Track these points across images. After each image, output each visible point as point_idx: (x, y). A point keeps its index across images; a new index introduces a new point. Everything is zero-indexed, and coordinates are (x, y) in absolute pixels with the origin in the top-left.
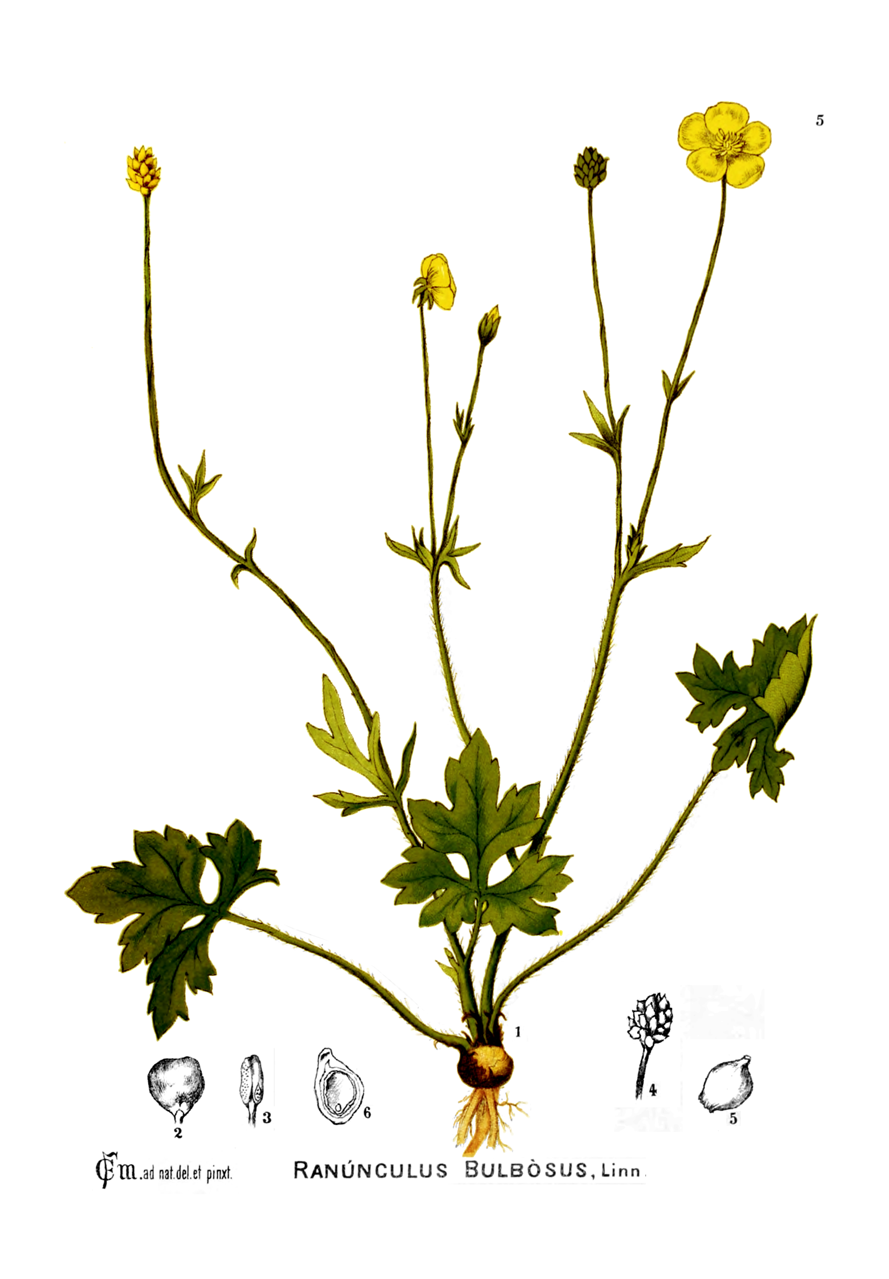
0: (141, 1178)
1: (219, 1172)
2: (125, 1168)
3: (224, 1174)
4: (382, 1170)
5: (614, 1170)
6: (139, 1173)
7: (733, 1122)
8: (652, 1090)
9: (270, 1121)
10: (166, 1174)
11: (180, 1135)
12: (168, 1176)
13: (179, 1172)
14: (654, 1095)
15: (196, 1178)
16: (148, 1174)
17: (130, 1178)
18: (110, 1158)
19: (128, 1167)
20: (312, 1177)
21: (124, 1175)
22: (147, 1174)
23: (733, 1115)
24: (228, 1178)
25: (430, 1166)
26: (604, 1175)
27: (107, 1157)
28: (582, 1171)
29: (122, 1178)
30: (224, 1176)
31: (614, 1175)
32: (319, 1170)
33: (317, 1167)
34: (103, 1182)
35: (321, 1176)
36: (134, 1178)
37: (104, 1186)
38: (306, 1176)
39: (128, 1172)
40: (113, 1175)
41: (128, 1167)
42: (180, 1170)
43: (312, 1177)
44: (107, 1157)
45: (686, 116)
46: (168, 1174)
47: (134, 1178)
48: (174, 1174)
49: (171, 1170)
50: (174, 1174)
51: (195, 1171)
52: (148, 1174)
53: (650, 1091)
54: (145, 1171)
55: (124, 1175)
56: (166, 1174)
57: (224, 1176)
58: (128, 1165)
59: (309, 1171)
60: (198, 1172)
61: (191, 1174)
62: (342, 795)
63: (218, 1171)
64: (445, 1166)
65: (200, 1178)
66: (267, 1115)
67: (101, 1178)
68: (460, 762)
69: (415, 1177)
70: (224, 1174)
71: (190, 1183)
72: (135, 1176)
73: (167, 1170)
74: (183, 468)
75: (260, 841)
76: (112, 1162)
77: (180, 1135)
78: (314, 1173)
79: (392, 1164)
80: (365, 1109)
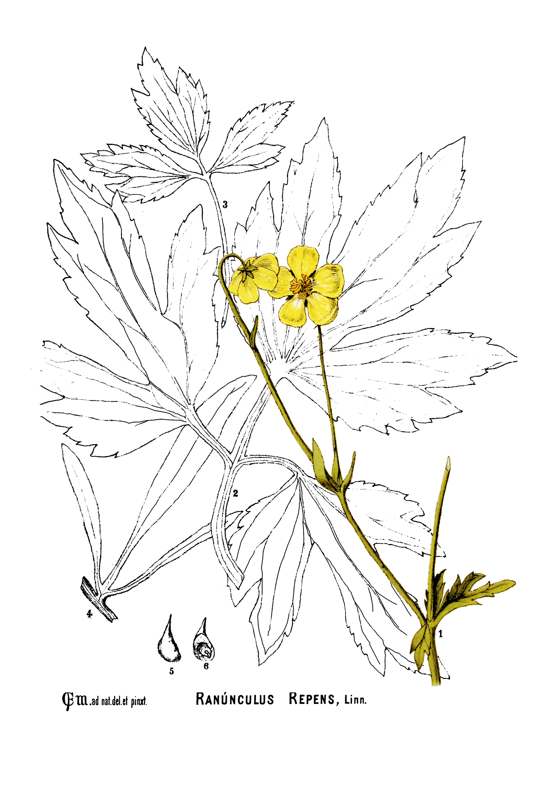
0: (90, 704)
1: (224, 702)
2: (80, 698)
3: (142, 702)
5: (351, 698)
6: (89, 701)
8: (89, 613)
9: (227, 206)
10: (106, 702)
11: (236, 494)
12: (107, 703)
13: (114, 701)
15: (124, 704)
16: (95, 702)
17: (80, 704)
19: (82, 697)
20: (206, 704)
21: (80, 702)
22: (94, 702)
23: (171, 669)
24: (145, 704)
26: (346, 703)
28: (332, 700)
29: (78, 704)
31: (351, 703)
33: (209, 697)
34: (66, 706)
35: (211, 704)
36: (86, 704)
37: (68, 710)
39: (82, 700)
40: (73, 702)
42: (114, 699)
43: (206, 704)
46: (107, 702)
47: (86, 704)
48: (111, 702)
49: (109, 699)
50: (111, 702)
51: (124, 699)
53: (87, 614)
54: (92, 700)
55: (80, 702)
56: (106, 702)
57: (142, 703)
58: (82, 696)
59: (205, 699)
60: (126, 700)
61: (121, 702)
62: (204, 97)
63: (138, 700)
67: (66, 704)
70: (142, 702)
71: (121, 707)
72: (87, 703)
73: (106, 699)
79: (255, 695)
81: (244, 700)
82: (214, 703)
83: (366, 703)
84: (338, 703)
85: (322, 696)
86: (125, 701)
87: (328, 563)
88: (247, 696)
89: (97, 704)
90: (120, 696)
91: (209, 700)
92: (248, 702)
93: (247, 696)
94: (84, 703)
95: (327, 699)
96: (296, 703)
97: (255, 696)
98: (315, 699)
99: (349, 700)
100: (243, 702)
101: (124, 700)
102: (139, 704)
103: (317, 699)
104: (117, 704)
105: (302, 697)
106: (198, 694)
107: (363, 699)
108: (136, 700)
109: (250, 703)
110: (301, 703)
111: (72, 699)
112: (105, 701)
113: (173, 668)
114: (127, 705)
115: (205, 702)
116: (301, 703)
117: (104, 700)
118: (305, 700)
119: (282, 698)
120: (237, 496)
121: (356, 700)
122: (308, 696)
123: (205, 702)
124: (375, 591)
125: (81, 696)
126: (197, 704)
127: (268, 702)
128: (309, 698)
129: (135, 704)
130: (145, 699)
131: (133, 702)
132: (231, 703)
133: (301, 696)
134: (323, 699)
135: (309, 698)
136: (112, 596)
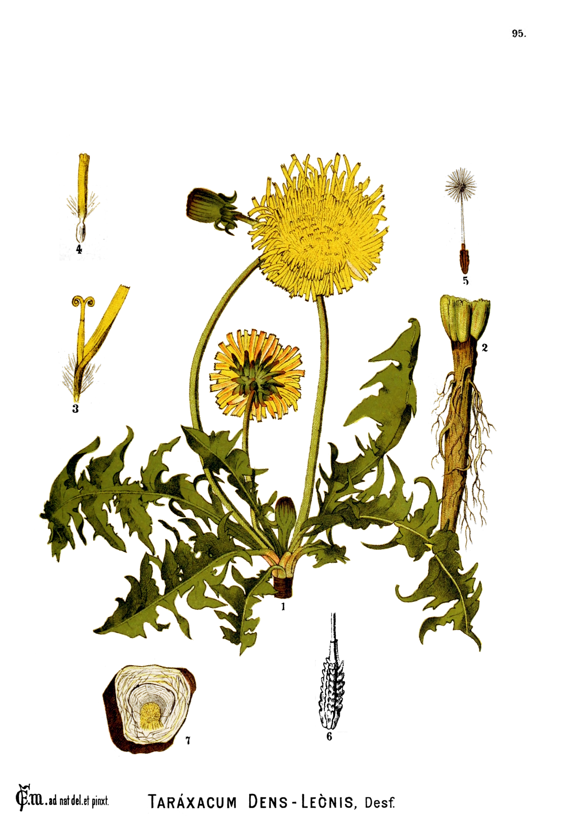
0: (46, 804)
2: (35, 797)
3: (103, 802)
4: (211, 803)
6: (45, 800)
9: (77, 411)
10: (65, 802)
11: (486, 349)
15: (85, 804)
16: (52, 802)
18: (25, 790)
19: (37, 796)
21: (34, 802)
25: (341, 798)
27: (23, 789)
30: (103, 803)
32: (202, 802)
33: (201, 799)
34: (20, 806)
35: (164, 807)
37: (21, 810)
38: (173, 807)
39: (37, 800)
44: (23, 789)
46: (66, 802)
47: (41, 803)
49: (68, 799)
51: (85, 799)
52: (52, 802)
53: (77, 250)
55: (34, 802)
56: (65, 802)
57: (103, 803)
61: (82, 802)
63: (99, 799)
64: (286, 800)
66: (76, 407)
68: (383, 431)
69: (307, 807)
70: (103, 802)
74: (322, 466)
75: (42, 516)
76: (26, 792)
77: (486, 349)
78: (179, 805)
81: (215, 803)
82: (168, 807)
84: (356, 807)
85: (271, 799)
88: (217, 798)
89: (56, 804)
90: (80, 795)
93: (217, 798)
94: (39, 802)
95: (278, 803)
97: (223, 798)
100: (213, 806)
103: (264, 802)
104: (77, 804)
105: (263, 800)
110: (312, 807)
111: (26, 798)
112: (64, 801)
116: (312, 807)
118: (316, 804)
119: (242, 802)
120: (486, 351)
127: (281, 805)
133: (262, 798)
134: (273, 802)
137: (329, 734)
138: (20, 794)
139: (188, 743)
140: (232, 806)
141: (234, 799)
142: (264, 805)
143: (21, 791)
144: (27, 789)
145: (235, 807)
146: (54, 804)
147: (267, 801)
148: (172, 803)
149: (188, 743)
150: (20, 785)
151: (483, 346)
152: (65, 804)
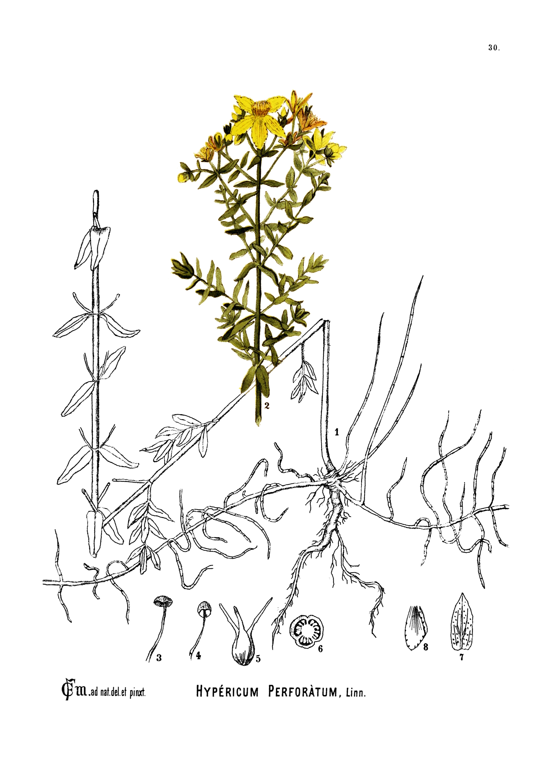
2: (79, 688)
3: (140, 693)
4: (239, 692)
6: (88, 692)
7: (258, 661)
9: (161, 659)
10: (105, 693)
11: (268, 407)
14: (199, 658)
16: (94, 693)
17: (79, 695)
18: (71, 683)
19: (81, 688)
21: (79, 693)
22: (93, 692)
24: (143, 695)
26: (347, 696)
27: (68, 682)
29: (78, 694)
30: (141, 694)
31: (352, 696)
36: (85, 695)
37: (67, 699)
38: (286, 695)
39: (81, 691)
41: (81, 688)
42: (113, 690)
43: (310, 696)
44: (68, 682)
45: (308, 216)
46: (106, 693)
47: (85, 695)
48: (110, 693)
49: (108, 690)
50: (110, 693)
51: (123, 690)
53: (197, 656)
54: (92, 691)
55: (79, 693)
56: (105, 693)
58: (82, 686)
60: (124, 691)
61: (120, 693)
63: (137, 691)
65: (125, 695)
70: (140, 693)
72: (86, 694)
73: (105, 690)
76: (72, 684)
78: (310, 694)
80: (319, 647)
83: (365, 696)
84: (340, 696)
86: (124, 692)
87: (373, 433)
88: (244, 689)
91: (312, 692)
92: (246, 694)
96: (230, 696)
98: (221, 692)
99: (349, 694)
100: (241, 694)
101: (123, 692)
102: (138, 696)
103: (222, 692)
104: (116, 695)
106: (270, 686)
107: (362, 691)
108: (134, 691)
109: (299, 695)
111: (71, 690)
112: (104, 692)
113: (259, 656)
114: (125, 695)
115: (308, 695)
117: (103, 690)
119: (263, 691)
120: (268, 408)
121: (356, 693)
122: (283, 688)
123: (308, 695)
124: (116, 510)
125: (80, 687)
126: (197, 696)
128: (215, 690)
129: (134, 696)
130: (143, 690)
131: (132, 693)
132: (330, 696)
135: (215, 690)
136: (332, 538)
137: (321, 647)
138: (66, 685)
139: (462, 659)
140: (254, 695)
141: (257, 689)
142: (222, 694)
143: (67, 683)
144: (73, 681)
145: (257, 696)
146: (96, 695)
147: (224, 691)
148: (285, 692)
149: (462, 659)
150: (67, 679)
151: (266, 404)
152: (105, 695)
